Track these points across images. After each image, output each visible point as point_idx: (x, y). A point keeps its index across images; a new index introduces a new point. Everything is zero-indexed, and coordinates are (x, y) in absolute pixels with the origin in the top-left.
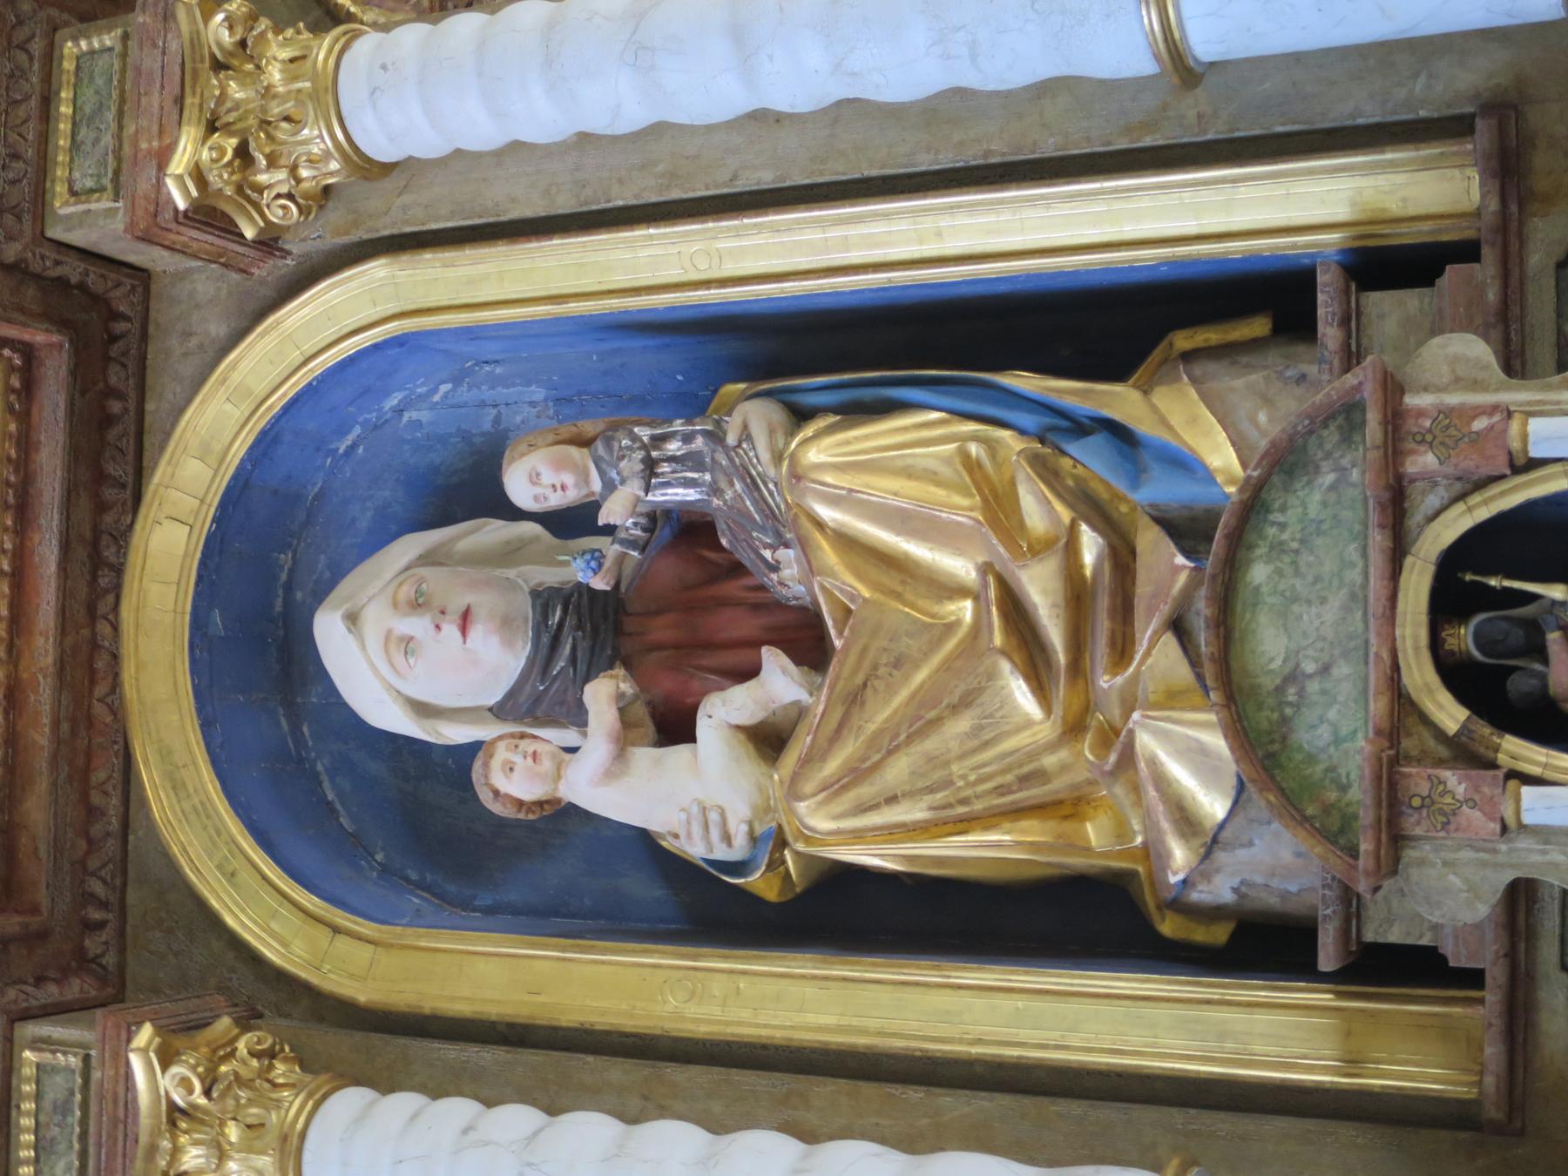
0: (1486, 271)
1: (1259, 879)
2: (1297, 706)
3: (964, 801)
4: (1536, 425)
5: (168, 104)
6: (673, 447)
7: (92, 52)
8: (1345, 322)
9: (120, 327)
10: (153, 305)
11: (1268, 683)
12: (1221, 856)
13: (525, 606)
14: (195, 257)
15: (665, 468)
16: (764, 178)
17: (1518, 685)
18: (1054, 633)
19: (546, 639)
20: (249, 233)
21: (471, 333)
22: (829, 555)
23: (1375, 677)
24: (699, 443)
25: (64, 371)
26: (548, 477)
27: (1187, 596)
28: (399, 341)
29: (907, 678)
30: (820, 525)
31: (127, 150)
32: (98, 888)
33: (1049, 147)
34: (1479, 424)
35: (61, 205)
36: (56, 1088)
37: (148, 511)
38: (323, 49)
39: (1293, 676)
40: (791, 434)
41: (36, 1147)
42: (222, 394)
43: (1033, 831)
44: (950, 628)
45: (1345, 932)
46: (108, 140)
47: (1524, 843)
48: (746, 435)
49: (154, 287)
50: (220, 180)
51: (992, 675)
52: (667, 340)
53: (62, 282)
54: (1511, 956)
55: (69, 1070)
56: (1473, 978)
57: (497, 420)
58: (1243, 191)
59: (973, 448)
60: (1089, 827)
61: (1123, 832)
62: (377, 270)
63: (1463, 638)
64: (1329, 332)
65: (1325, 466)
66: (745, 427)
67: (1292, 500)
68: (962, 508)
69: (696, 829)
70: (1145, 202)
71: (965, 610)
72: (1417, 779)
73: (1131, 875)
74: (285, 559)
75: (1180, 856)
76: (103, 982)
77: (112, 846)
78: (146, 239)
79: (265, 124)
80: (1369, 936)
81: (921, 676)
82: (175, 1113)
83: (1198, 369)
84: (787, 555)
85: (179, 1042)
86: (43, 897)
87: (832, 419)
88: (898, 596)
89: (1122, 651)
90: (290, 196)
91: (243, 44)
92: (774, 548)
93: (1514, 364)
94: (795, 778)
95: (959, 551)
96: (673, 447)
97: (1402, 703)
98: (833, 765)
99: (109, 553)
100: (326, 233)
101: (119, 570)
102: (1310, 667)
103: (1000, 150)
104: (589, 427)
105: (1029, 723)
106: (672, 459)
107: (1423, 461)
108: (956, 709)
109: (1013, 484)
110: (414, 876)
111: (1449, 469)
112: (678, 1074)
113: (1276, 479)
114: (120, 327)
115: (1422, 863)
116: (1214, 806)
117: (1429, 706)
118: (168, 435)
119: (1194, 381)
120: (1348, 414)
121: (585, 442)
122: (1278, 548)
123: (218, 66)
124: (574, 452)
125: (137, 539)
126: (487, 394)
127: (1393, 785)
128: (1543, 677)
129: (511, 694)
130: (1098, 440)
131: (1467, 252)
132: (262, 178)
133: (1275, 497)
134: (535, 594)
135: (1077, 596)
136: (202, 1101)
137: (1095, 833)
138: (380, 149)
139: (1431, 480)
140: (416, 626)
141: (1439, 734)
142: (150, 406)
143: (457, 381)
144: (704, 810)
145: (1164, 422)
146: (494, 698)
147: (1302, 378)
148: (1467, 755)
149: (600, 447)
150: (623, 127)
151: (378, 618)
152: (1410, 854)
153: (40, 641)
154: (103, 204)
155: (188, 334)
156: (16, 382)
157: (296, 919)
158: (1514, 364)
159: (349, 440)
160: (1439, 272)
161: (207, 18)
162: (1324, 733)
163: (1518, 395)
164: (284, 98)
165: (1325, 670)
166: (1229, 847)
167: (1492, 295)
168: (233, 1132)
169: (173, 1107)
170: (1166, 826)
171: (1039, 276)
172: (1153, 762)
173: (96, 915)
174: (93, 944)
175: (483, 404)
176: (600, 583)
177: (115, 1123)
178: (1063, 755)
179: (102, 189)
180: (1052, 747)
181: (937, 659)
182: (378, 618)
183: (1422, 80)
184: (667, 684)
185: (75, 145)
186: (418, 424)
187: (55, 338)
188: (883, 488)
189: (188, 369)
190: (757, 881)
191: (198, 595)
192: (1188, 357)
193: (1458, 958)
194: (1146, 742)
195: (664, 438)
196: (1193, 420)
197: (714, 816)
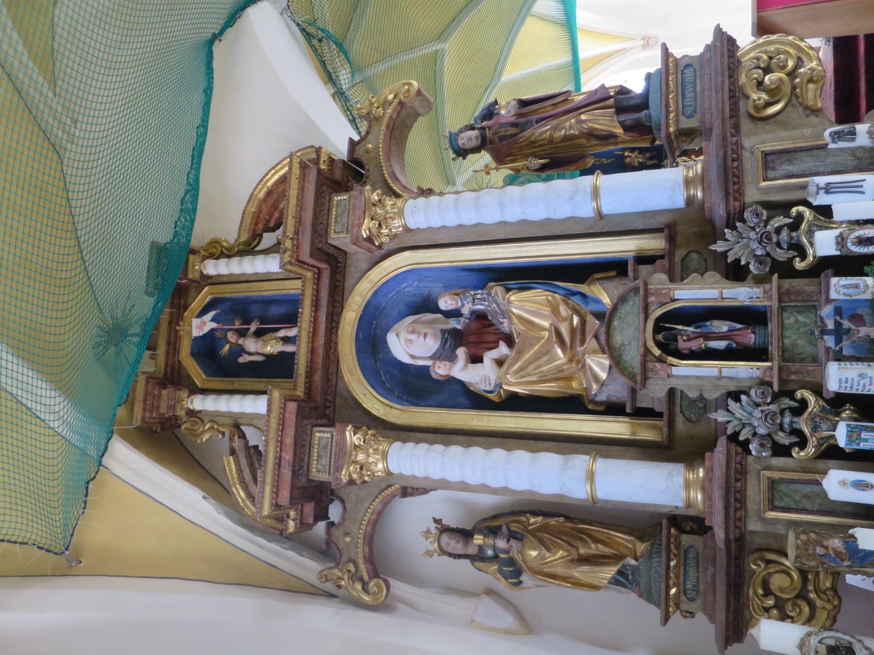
0: (666, 261)
1: (612, 394)
2: (624, 351)
3: (545, 376)
4: (676, 292)
5: (361, 213)
6: (479, 296)
7: (341, 200)
8: (634, 271)
9: (340, 265)
10: (348, 260)
11: (617, 346)
12: (604, 388)
13: (439, 333)
14: (363, 249)
15: (477, 301)
16: (502, 236)
17: (672, 347)
18: (567, 338)
19: (444, 340)
20: (377, 244)
21: (428, 269)
22: (515, 321)
23: (641, 344)
24: (485, 296)
25: (328, 274)
26: (449, 302)
27: (598, 330)
28: (410, 271)
29: (533, 348)
30: (514, 314)
31: (350, 223)
32: (330, 398)
33: (568, 232)
34: (664, 291)
35: (333, 235)
36: (324, 442)
37: (346, 309)
38: (399, 202)
39: (623, 345)
40: (506, 294)
41: (318, 457)
42: (366, 282)
43: (562, 383)
44: (543, 338)
45: (632, 403)
46: (345, 220)
47: (673, 379)
48: (496, 294)
49: (348, 256)
50: (374, 231)
51: (553, 347)
52: (472, 273)
53: (329, 254)
54: (669, 409)
55: (327, 438)
56: (660, 415)
57: (429, 291)
58: (612, 243)
59: (549, 298)
60: (573, 384)
61: (581, 384)
62: (407, 254)
63: (660, 337)
64: (631, 274)
65: (631, 300)
66: (496, 292)
67: (623, 308)
68: (547, 311)
69: (483, 382)
70: (589, 244)
71: (546, 334)
72: (650, 365)
73: (582, 395)
74: (375, 322)
75: (595, 387)
76: (329, 421)
77: (333, 388)
78: (355, 244)
79: (385, 218)
80: (638, 405)
81: (536, 348)
82: (356, 447)
83: (600, 281)
84: (505, 320)
85: (357, 430)
86: (318, 398)
87: (516, 291)
88: (531, 330)
89: (583, 342)
90: (388, 236)
91: (380, 200)
92: (503, 319)
93: (672, 280)
94: (507, 370)
95: (545, 320)
96: (479, 296)
97: (647, 351)
98: (516, 367)
99: (335, 319)
100: (395, 245)
101: (338, 323)
102: (626, 343)
103: (557, 232)
104: (459, 291)
105: (560, 359)
106: (478, 299)
107: (652, 299)
108: (544, 355)
109: (558, 305)
110: (405, 398)
111: (657, 301)
112: (476, 439)
113: (620, 303)
114: (340, 265)
115: (650, 384)
116: (603, 376)
117: (652, 350)
118: (352, 291)
119: (600, 284)
120: (636, 290)
121: (457, 295)
122: (620, 318)
123: (374, 205)
124: (455, 297)
125: (343, 315)
126: (427, 285)
127: (645, 366)
128: (677, 346)
129: (435, 354)
130: (578, 296)
131: (662, 257)
132: (382, 231)
133: (620, 307)
134: (441, 331)
135: (573, 331)
136: (363, 444)
137: (575, 385)
138: (412, 225)
139: (653, 303)
140: (413, 337)
141: (654, 356)
142: (346, 284)
143: (419, 281)
144: (485, 377)
145: (593, 292)
146: (429, 355)
147: (624, 284)
148: (660, 360)
149: (462, 296)
150: (471, 223)
151: (404, 335)
152: (648, 382)
153: (320, 338)
154: (344, 235)
155: (356, 267)
156: (316, 277)
157: (381, 405)
158: (672, 280)
159: (392, 295)
160: (655, 261)
161: (372, 193)
162: (629, 357)
163: (672, 286)
164: (391, 213)
165: (630, 343)
166: (606, 386)
167: (667, 266)
168: (371, 451)
169: (355, 445)
170: (592, 380)
171: (559, 261)
172: (590, 366)
173: (329, 405)
174: (327, 412)
175: (426, 287)
176: (459, 327)
177: (340, 449)
178: (568, 366)
179: (343, 232)
180: (565, 364)
181: (540, 344)
182: (404, 335)
183: (652, 220)
184: (474, 351)
185: (336, 221)
186: (409, 291)
187: (327, 266)
188: (530, 306)
189: (357, 275)
190: (493, 397)
191: (357, 329)
192: (598, 279)
193: (657, 409)
194: (588, 361)
195: (477, 294)
196: (600, 292)
197: (488, 378)
